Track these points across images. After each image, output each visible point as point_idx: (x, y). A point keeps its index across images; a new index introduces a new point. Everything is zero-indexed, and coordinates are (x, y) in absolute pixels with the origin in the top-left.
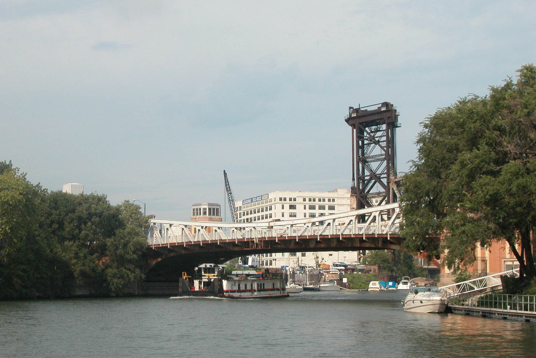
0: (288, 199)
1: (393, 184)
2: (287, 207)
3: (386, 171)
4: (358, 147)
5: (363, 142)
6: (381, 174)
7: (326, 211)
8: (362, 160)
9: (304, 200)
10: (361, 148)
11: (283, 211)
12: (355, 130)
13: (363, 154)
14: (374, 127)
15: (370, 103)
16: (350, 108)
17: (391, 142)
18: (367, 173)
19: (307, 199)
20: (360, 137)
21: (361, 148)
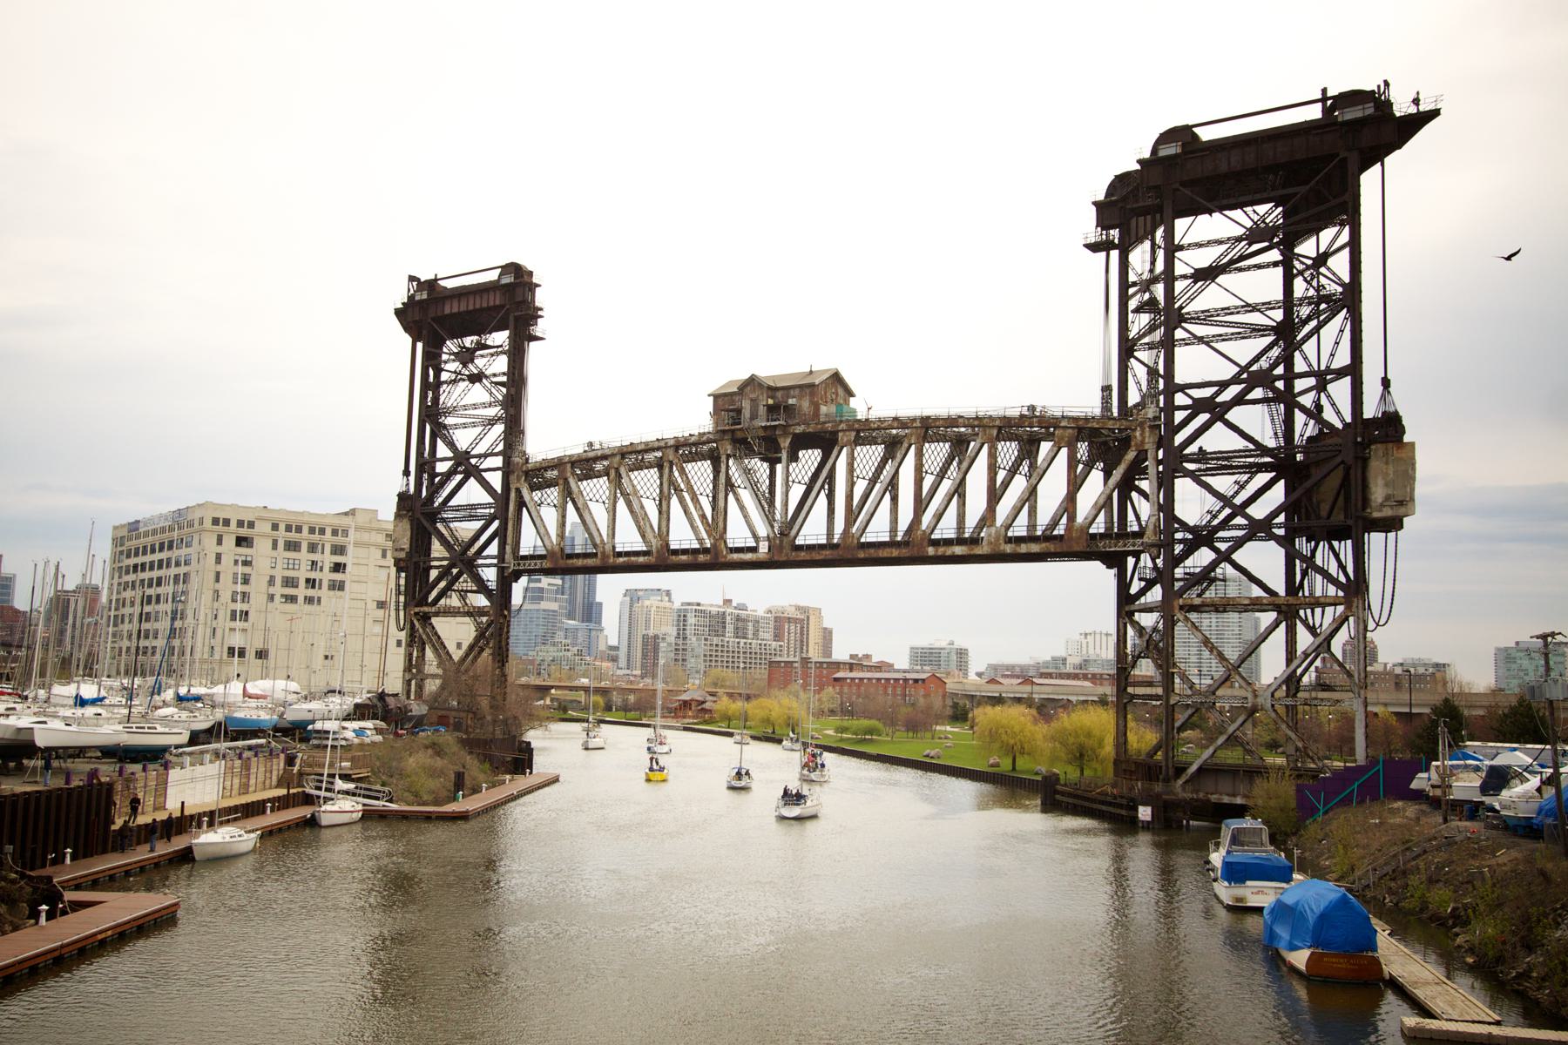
0: (233, 524)
1: (518, 479)
2: (229, 541)
3: (501, 447)
4: (425, 385)
5: (437, 376)
6: (486, 456)
7: (303, 574)
8: (431, 416)
9: (275, 527)
10: (431, 387)
11: (219, 549)
12: (420, 345)
13: (436, 399)
14: (469, 341)
15: (465, 262)
16: (412, 279)
17: (516, 382)
18: (443, 450)
19: (282, 527)
20: (432, 359)
21: (431, 387)
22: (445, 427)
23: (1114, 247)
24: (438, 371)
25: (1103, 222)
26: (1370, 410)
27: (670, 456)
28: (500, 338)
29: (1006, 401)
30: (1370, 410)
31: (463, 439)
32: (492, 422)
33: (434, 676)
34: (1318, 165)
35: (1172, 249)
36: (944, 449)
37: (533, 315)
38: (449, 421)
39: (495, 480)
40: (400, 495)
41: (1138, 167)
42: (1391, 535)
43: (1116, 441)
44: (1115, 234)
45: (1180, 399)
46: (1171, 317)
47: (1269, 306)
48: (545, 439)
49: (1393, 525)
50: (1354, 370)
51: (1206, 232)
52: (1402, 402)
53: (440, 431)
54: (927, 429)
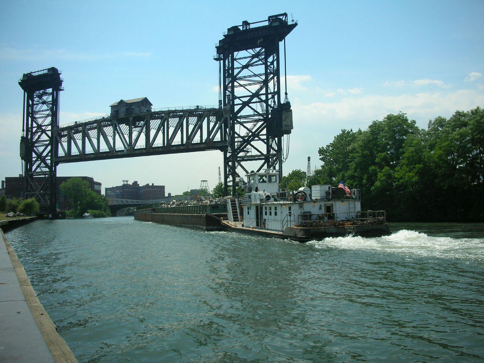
15: (38, 66)
17: (55, 102)
18: (35, 125)
20: (30, 97)
22: (35, 118)
23: (222, 59)
24: (33, 101)
25: (218, 52)
26: (282, 102)
27: (99, 124)
28: (50, 90)
29: (189, 105)
30: (282, 102)
31: (40, 121)
32: (48, 115)
33: (35, 157)
34: (268, 38)
35: (233, 60)
36: (195, 119)
37: (60, 82)
38: (37, 116)
39: (49, 133)
40: (22, 137)
41: (224, 37)
42: (288, 135)
43: (226, 115)
44: (222, 55)
45: (237, 101)
46: (234, 79)
47: (260, 75)
48: (66, 119)
49: (289, 132)
50: (278, 93)
51: (242, 56)
52: (290, 100)
53: (34, 119)
54: (189, 113)
